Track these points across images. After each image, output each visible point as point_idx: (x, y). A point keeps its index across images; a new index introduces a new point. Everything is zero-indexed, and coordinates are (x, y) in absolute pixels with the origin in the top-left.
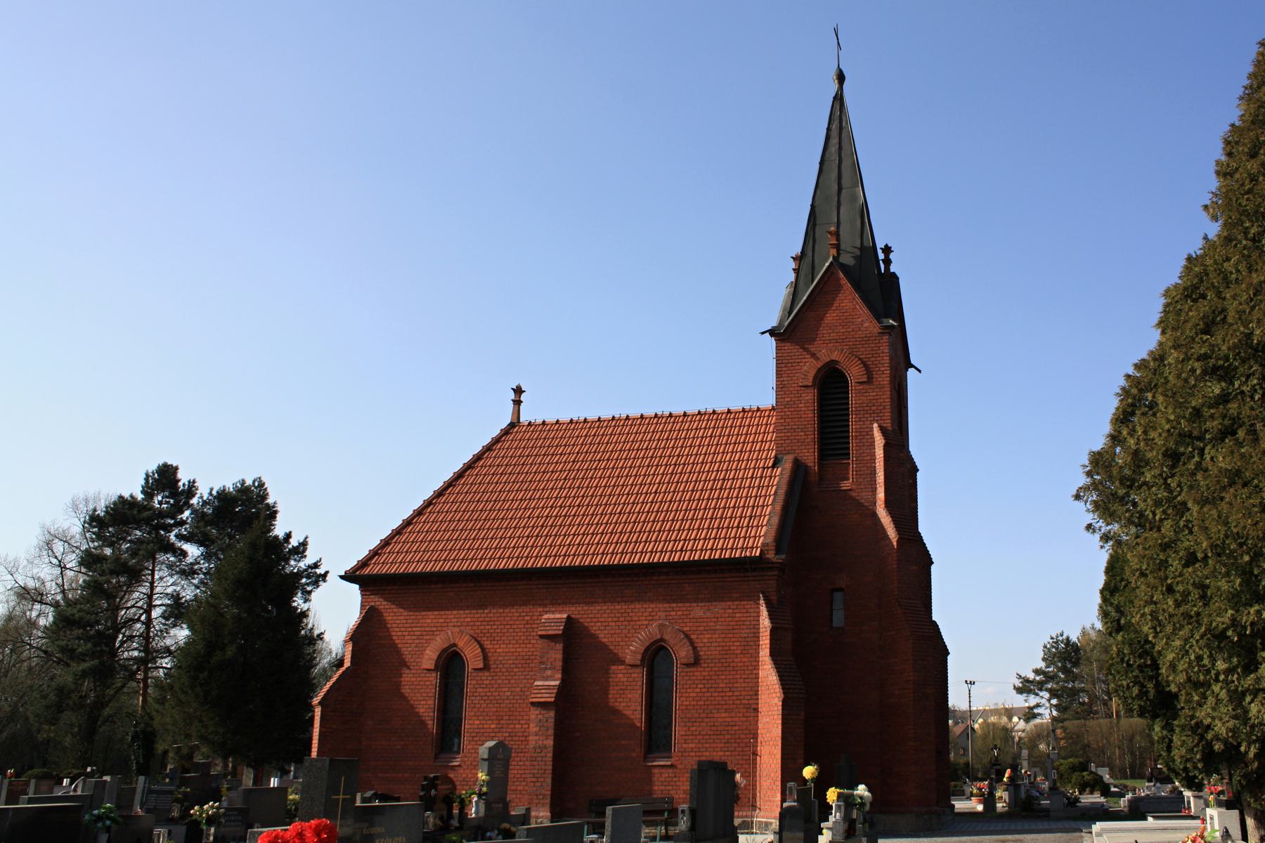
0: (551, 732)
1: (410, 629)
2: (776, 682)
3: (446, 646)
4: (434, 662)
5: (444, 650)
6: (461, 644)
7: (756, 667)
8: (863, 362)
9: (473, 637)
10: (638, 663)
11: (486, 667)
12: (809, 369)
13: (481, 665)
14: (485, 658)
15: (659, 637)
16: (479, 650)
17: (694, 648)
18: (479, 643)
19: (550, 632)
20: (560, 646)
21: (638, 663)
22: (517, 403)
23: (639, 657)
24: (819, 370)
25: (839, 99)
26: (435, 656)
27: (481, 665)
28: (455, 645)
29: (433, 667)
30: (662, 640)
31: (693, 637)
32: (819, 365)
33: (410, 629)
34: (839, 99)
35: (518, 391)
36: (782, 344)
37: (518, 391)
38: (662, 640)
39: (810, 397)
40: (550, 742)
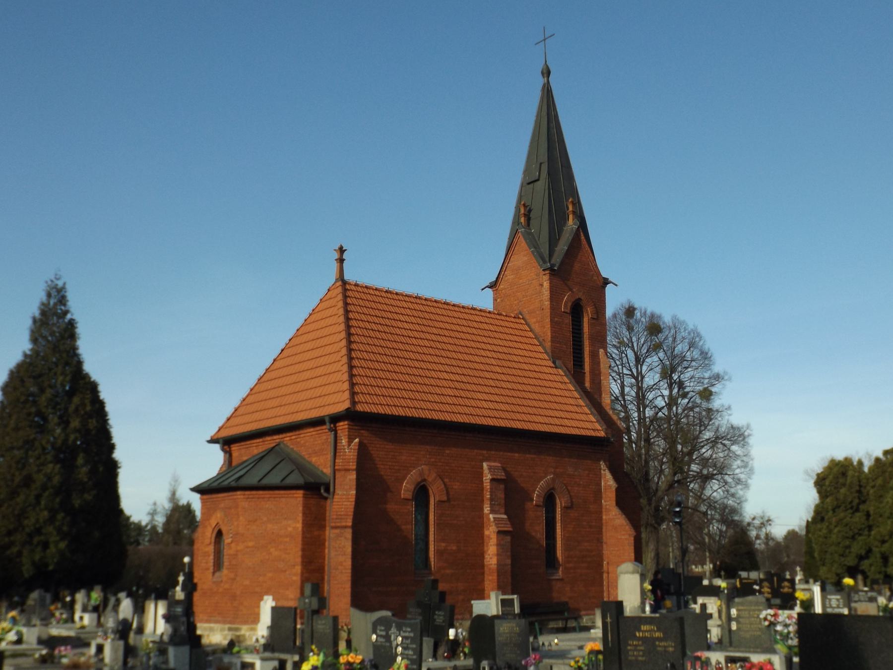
0: (509, 554)
1: (390, 464)
2: (625, 524)
3: (419, 480)
4: (411, 493)
5: (419, 483)
6: (430, 479)
7: (600, 512)
8: (595, 305)
9: (439, 476)
10: (541, 504)
11: (449, 500)
12: (566, 299)
13: (445, 498)
14: (448, 493)
15: (552, 486)
16: (443, 486)
17: (570, 496)
18: (442, 480)
19: (499, 477)
20: (502, 486)
21: (541, 504)
22: (341, 261)
23: (542, 500)
24: (573, 303)
25: (548, 94)
26: (412, 487)
27: (445, 498)
28: (425, 480)
29: (410, 497)
30: (553, 489)
31: (569, 488)
32: (573, 300)
33: (390, 464)
34: (548, 94)
35: (342, 250)
36: (552, 278)
37: (342, 250)
38: (553, 489)
39: (568, 320)
40: (509, 561)
